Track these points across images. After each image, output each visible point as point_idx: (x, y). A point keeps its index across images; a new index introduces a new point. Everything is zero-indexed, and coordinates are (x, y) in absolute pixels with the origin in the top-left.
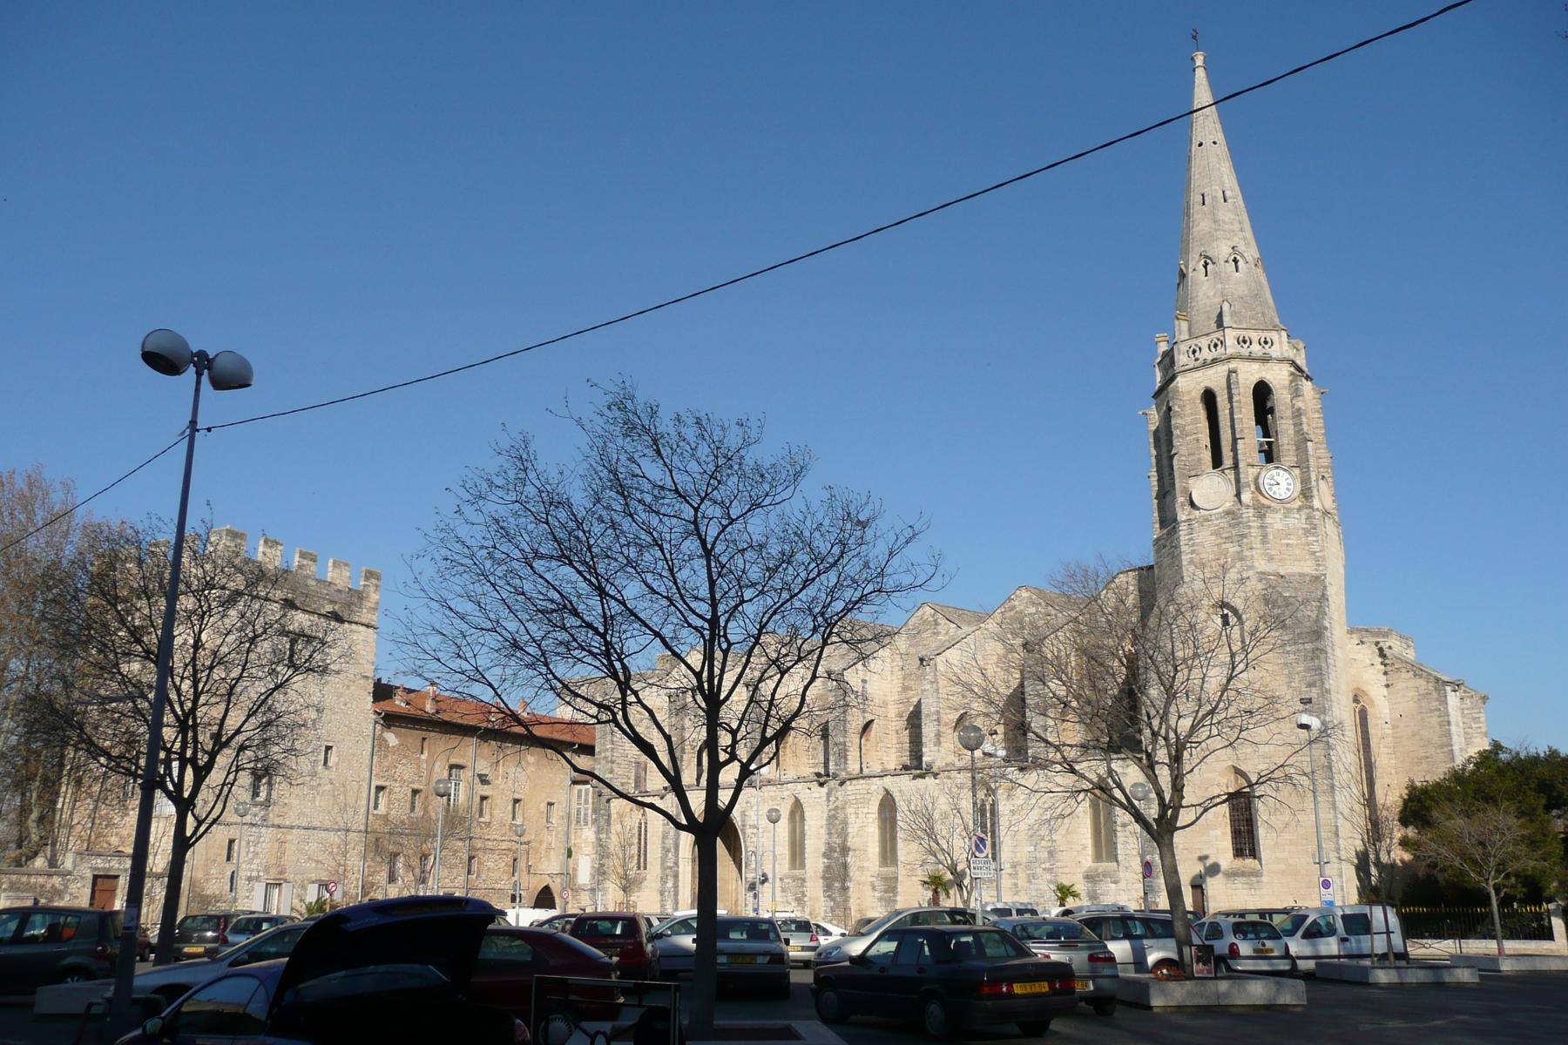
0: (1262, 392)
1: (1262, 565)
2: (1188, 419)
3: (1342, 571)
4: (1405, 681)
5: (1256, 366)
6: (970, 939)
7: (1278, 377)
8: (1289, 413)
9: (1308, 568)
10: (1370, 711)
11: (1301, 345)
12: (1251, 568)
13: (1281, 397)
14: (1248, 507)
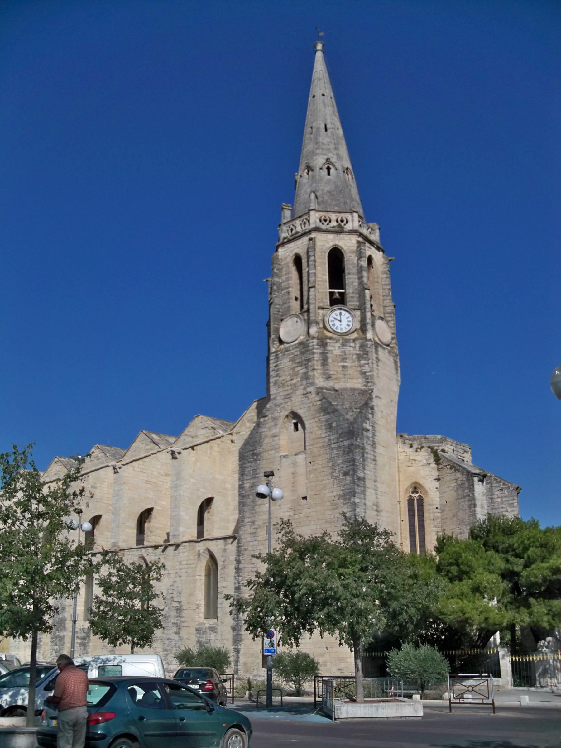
0: (336, 257)
1: (320, 382)
2: (284, 278)
3: (396, 389)
4: (450, 476)
5: (331, 236)
6: (483, 675)
7: (348, 243)
8: (355, 270)
9: (358, 383)
10: (426, 500)
11: (376, 227)
12: (312, 384)
13: (351, 261)
14: (313, 338)
